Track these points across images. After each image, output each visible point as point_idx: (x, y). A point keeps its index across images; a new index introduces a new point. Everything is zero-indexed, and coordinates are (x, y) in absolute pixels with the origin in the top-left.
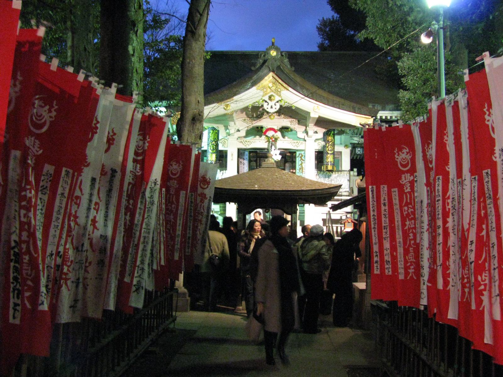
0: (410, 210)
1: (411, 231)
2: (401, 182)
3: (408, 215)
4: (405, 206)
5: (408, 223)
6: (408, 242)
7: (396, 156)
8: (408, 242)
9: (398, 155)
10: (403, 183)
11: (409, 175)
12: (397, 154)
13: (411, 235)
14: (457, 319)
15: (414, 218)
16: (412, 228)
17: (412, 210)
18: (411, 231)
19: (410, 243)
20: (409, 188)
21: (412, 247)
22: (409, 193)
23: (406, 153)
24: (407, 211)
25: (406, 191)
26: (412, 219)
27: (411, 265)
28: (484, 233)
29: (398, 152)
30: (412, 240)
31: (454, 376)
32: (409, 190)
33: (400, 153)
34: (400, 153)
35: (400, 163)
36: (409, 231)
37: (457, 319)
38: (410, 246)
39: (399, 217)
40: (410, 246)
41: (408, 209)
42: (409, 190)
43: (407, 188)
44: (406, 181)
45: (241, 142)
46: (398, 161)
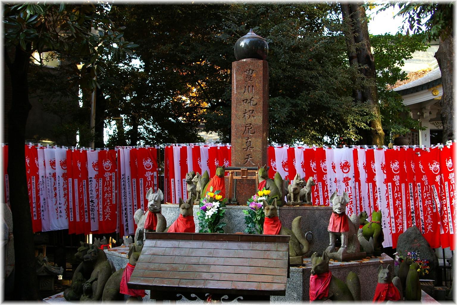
0: (428, 195)
1: (429, 206)
2: (436, 181)
3: (107, 191)
4: (147, 187)
5: (426, 202)
6: (106, 204)
7: (271, 163)
8: (106, 204)
9: (431, 166)
10: (325, 179)
11: (150, 172)
12: (430, 166)
13: (108, 200)
14: (439, 265)
15: (431, 199)
16: (109, 197)
17: (430, 195)
18: (429, 206)
19: (428, 213)
20: (427, 183)
21: (108, 206)
22: (109, 181)
23: (436, 164)
24: (397, 195)
25: (425, 185)
26: (400, 200)
27: (429, 224)
28: (417, 204)
29: (431, 165)
30: (400, 211)
31: (305, 298)
32: (150, 179)
33: (432, 165)
34: (432, 165)
35: (393, 169)
36: (427, 206)
37: (439, 265)
38: (428, 214)
39: (322, 199)
40: (107, 205)
41: (427, 194)
42: (398, 184)
43: (426, 183)
44: (397, 179)
45: (433, 124)
46: (432, 170)
